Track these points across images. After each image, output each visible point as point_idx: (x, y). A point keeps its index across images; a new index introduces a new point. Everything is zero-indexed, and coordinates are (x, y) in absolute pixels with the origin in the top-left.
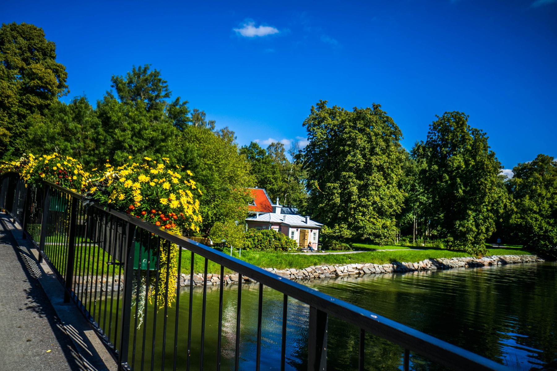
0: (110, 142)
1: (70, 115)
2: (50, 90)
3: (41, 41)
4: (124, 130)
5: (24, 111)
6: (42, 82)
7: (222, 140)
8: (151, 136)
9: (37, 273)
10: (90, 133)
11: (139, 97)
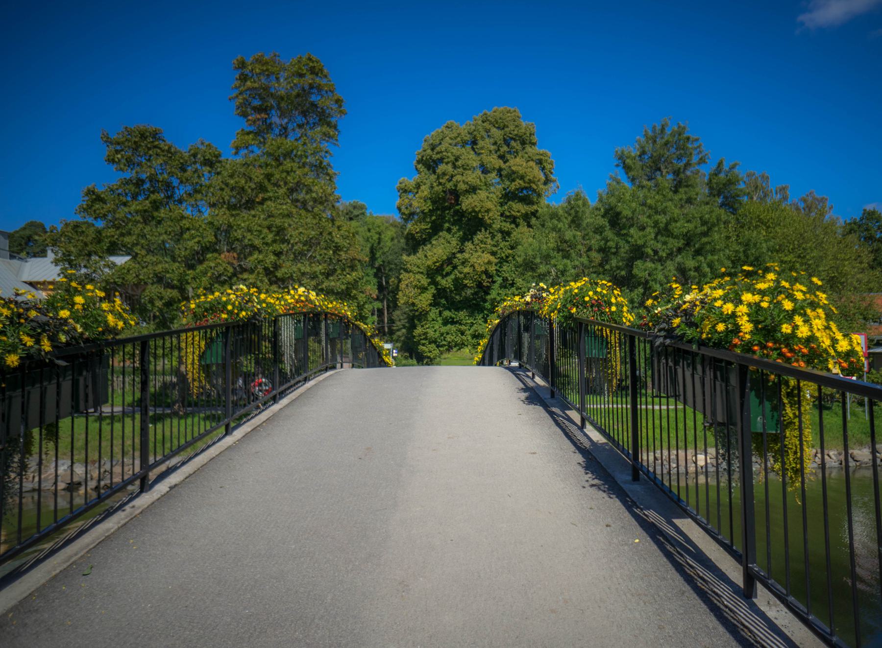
0: (625, 248)
1: (565, 220)
2: (534, 191)
3: (517, 126)
4: (643, 228)
5: (507, 226)
6: (525, 182)
7: (808, 215)
8: (685, 230)
9: (587, 444)
10: (595, 241)
11: (658, 173)
